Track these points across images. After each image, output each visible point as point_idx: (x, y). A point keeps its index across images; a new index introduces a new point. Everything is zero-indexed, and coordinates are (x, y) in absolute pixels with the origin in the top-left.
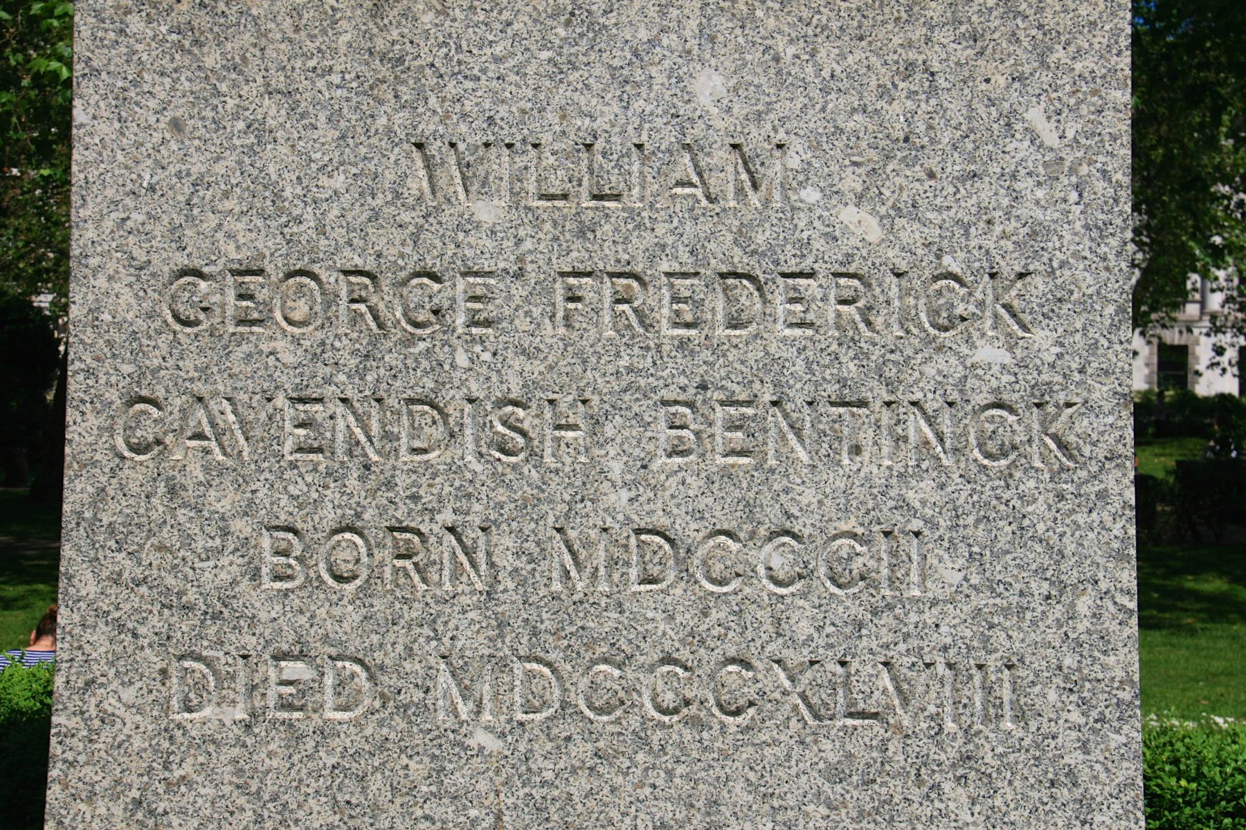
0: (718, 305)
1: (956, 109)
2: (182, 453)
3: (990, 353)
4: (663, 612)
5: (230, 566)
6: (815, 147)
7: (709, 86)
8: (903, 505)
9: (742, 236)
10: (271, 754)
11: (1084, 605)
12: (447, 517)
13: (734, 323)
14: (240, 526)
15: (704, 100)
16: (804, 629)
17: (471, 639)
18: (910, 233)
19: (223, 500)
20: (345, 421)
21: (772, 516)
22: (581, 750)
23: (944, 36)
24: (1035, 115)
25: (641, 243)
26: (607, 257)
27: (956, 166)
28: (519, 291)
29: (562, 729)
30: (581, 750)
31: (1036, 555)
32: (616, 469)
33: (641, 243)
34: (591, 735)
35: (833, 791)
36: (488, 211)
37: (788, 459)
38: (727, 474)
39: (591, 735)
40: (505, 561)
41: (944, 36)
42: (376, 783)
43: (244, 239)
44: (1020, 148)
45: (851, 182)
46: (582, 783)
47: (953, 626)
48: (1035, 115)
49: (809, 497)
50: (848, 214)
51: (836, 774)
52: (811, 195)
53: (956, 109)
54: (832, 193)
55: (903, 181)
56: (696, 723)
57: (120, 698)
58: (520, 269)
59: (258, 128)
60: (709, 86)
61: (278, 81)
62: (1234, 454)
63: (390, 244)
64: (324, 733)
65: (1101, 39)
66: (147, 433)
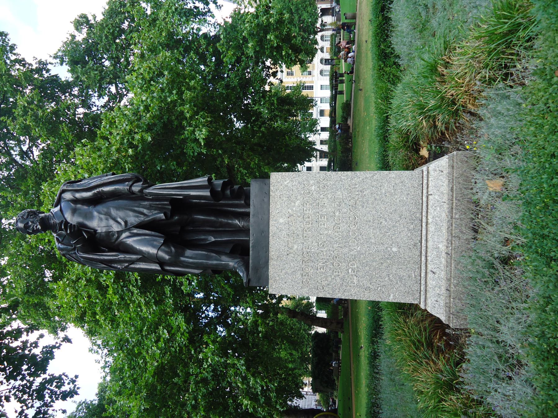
0: (307, 219)
1: (285, 192)
2: (324, 283)
3: (313, 188)
4: (343, 227)
5: (337, 278)
6: (289, 208)
7: (281, 220)
8: (331, 198)
9: (299, 217)
10: (360, 274)
11: (343, 178)
12: (332, 252)
13: (309, 218)
14: (333, 277)
15: (283, 221)
16: (346, 210)
17: (346, 250)
18: (299, 197)
19: (330, 279)
20: (320, 264)
21: (332, 214)
22: (360, 237)
23: (276, 193)
24: (286, 183)
25: (300, 229)
26: (301, 233)
27: (291, 192)
28: (305, 243)
29: (358, 239)
30: (360, 237)
31: (337, 183)
32: (326, 232)
33: (300, 229)
34: (358, 236)
35: (365, 207)
36: (296, 247)
37: (325, 212)
38: (327, 219)
39: (358, 236)
40: (337, 245)
41: (276, 193)
42: (364, 261)
43: (298, 275)
44: (289, 185)
45: (293, 204)
46: (364, 237)
47: (345, 193)
48: (286, 183)
49: (330, 209)
50: (297, 204)
51: (363, 207)
52: (294, 209)
53: (285, 192)
54: (294, 206)
55: (293, 198)
56: (357, 223)
57: (353, 291)
58: (532, 386)
59: (286, 273)
60: (281, 220)
61: (280, 271)
62: (309, 399)
63: (299, 258)
64: (358, 267)
65: (277, 176)
66: (321, 288)
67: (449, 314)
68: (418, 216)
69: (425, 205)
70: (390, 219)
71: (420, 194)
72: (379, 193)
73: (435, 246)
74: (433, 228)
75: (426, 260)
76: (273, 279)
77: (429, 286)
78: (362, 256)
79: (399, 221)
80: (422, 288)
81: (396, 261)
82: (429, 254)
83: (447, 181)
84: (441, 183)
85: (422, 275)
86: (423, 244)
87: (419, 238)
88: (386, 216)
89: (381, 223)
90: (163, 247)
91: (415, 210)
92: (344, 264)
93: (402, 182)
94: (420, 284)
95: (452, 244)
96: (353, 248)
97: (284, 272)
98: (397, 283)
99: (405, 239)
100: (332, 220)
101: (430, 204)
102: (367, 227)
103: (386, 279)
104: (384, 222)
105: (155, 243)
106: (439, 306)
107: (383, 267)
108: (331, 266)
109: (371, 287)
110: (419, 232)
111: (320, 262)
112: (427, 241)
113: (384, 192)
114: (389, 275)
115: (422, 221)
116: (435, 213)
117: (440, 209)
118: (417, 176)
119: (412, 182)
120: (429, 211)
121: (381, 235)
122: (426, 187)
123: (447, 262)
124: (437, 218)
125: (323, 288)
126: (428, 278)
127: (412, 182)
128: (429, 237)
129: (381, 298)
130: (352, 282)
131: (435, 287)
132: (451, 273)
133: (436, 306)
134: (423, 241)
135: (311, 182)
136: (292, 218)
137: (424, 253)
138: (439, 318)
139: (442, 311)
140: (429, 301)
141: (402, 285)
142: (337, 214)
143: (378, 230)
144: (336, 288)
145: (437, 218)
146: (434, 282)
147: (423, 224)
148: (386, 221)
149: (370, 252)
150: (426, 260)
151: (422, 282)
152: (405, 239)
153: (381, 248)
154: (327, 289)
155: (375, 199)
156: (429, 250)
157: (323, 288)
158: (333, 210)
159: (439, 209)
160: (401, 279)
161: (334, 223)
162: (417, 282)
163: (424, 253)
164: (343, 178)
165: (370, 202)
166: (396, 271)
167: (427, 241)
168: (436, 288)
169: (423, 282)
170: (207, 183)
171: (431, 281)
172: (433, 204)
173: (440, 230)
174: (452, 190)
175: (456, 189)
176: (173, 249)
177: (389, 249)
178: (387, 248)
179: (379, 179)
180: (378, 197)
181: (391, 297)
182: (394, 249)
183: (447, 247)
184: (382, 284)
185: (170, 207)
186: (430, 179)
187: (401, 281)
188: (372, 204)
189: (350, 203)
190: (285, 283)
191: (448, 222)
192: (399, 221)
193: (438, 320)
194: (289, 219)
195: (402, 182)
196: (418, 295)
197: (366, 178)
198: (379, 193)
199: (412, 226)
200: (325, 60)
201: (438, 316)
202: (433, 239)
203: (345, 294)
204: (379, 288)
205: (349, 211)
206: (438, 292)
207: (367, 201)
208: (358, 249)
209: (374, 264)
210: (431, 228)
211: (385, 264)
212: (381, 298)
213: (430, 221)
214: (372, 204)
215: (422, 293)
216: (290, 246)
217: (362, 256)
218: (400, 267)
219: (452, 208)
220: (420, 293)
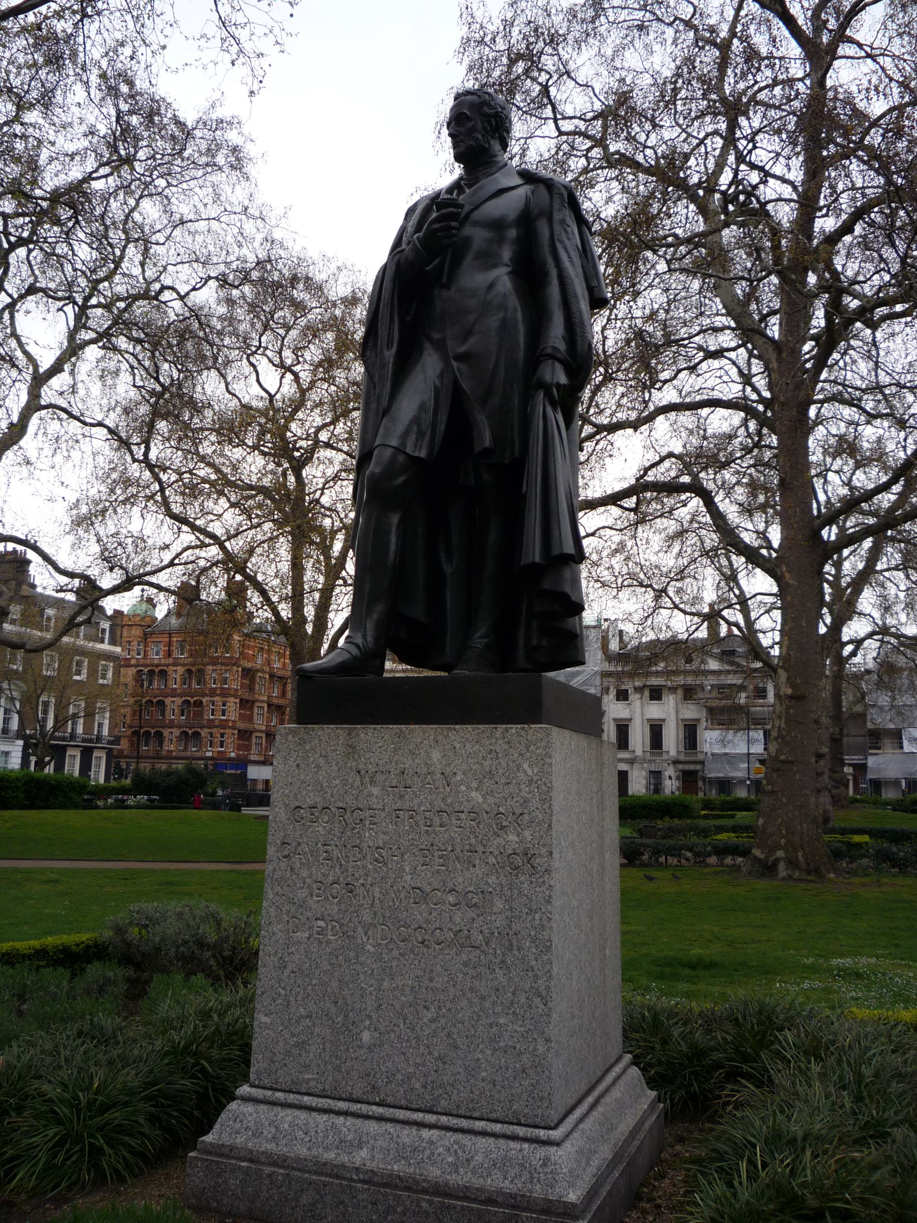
1: (504, 764)
3: (513, 837)
5: (305, 892)
7: (436, 755)
8: (487, 883)
12: (362, 881)
14: (308, 881)
16: (458, 920)
17: (367, 918)
18: (490, 800)
19: (304, 873)
20: (336, 852)
21: (450, 885)
22: (395, 953)
24: (525, 766)
26: (407, 805)
27: (503, 781)
28: (383, 815)
29: (390, 947)
30: (395, 953)
32: (407, 869)
34: (398, 948)
36: (375, 791)
37: (455, 868)
38: (438, 871)
39: (398, 948)
40: (377, 895)
42: (341, 958)
44: (521, 775)
45: (474, 784)
46: (394, 963)
48: (525, 766)
49: (461, 880)
50: (474, 794)
51: (465, 964)
52: (463, 788)
54: (469, 787)
59: (318, 767)
60: (436, 755)
61: (324, 753)
63: (350, 800)
64: (328, 942)
67: (218, 1150)
68: (443, 1102)
69: (464, 1123)
70: (435, 1031)
71: (493, 1116)
72: (498, 1009)
73: (365, 1139)
74: (406, 1140)
75: (339, 1113)
76: (306, 736)
77: (282, 1113)
78: (352, 954)
79: (430, 1053)
80: (279, 1095)
81: (341, 1037)
82: (350, 1121)
83: (515, 1190)
84: (512, 1173)
85: (306, 1098)
86: (374, 1108)
87: (390, 1100)
88: (443, 1021)
89: (428, 1009)
90: (401, 458)
91: (455, 1097)
92: (336, 909)
93: (524, 1071)
94: (291, 1091)
95: (364, 1182)
96: (370, 933)
97: (322, 761)
98: (293, 1035)
99: (390, 1064)
100: (436, 885)
101: (466, 1139)
102: (419, 972)
103: (301, 1010)
104: (430, 1016)
105: (413, 437)
106: (237, 1132)
107: (328, 1005)
108: (331, 879)
109: (287, 972)
110: (403, 1102)
111: (341, 852)
112: (381, 1119)
113: (502, 1021)
114: (309, 1016)
115: (430, 1111)
116: (441, 1150)
117: (450, 1164)
118: (540, 1112)
119: (525, 1096)
120: (449, 1134)
121: (398, 1007)
122: (509, 1133)
123: (325, 1164)
124: (428, 1152)
125: (285, 857)
126: (298, 1113)
127: (525, 1096)
128: (389, 1126)
129: (263, 993)
130: (297, 926)
131: (276, 1127)
132: (299, 1170)
133: (245, 1124)
134: (380, 1110)
135: (527, 833)
136: (441, 782)
137: (355, 1107)
138: (211, 1128)
139: (226, 1139)
140: (250, 1108)
141: (288, 1047)
142: (451, 899)
143: (411, 998)
144: (286, 888)
145: (428, 1152)
146: (286, 1126)
147: (421, 1115)
148: (432, 1021)
149: (362, 977)
150: (339, 1113)
151: (292, 1096)
152: (390, 1064)
153: (371, 1004)
154: (283, 865)
155: (483, 998)
156: (358, 1122)
157: (285, 857)
158: (459, 889)
159: (450, 1160)
160: (302, 1045)
161: (428, 889)
162: (293, 1083)
163: (355, 1107)
164: (537, 916)
165: (476, 983)
166: (318, 1035)
167: (381, 1119)
168: (273, 1130)
169: (292, 1098)
170: (556, 551)
171: (289, 1118)
172: (462, 1147)
173: (398, 1158)
174: (490, 1201)
175: (489, 1212)
176: (401, 480)
177: (367, 1023)
178: (370, 1017)
179: (533, 1011)
180: (487, 1004)
181: (264, 1019)
182: (366, 1036)
183: (357, 1169)
184: (292, 999)
185: (507, 461)
186: (526, 1145)
187: (296, 1045)
188: (472, 989)
189: (474, 933)
190: (298, 766)
191: (414, 1179)
192: (430, 1053)
193: (207, 1128)
194: (439, 776)
195: (524, 1071)
196: (266, 1082)
197: (536, 977)
198: (498, 1009)
199: (417, 1086)
200: (623, 923)
201: (217, 1126)
202: (383, 1136)
203: (272, 910)
204: (283, 992)
205: (456, 928)
206: (265, 1133)
207: (479, 976)
208: (369, 947)
209: (335, 984)
210: (407, 1135)
211: (333, 1010)
212: (263, 993)
213: (426, 1134)
214: (472, 989)
215: (270, 1093)
216: (379, 778)
217: (352, 954)
218: (328, 1045)
219: (447, 1195)
220: (271, 1089)
